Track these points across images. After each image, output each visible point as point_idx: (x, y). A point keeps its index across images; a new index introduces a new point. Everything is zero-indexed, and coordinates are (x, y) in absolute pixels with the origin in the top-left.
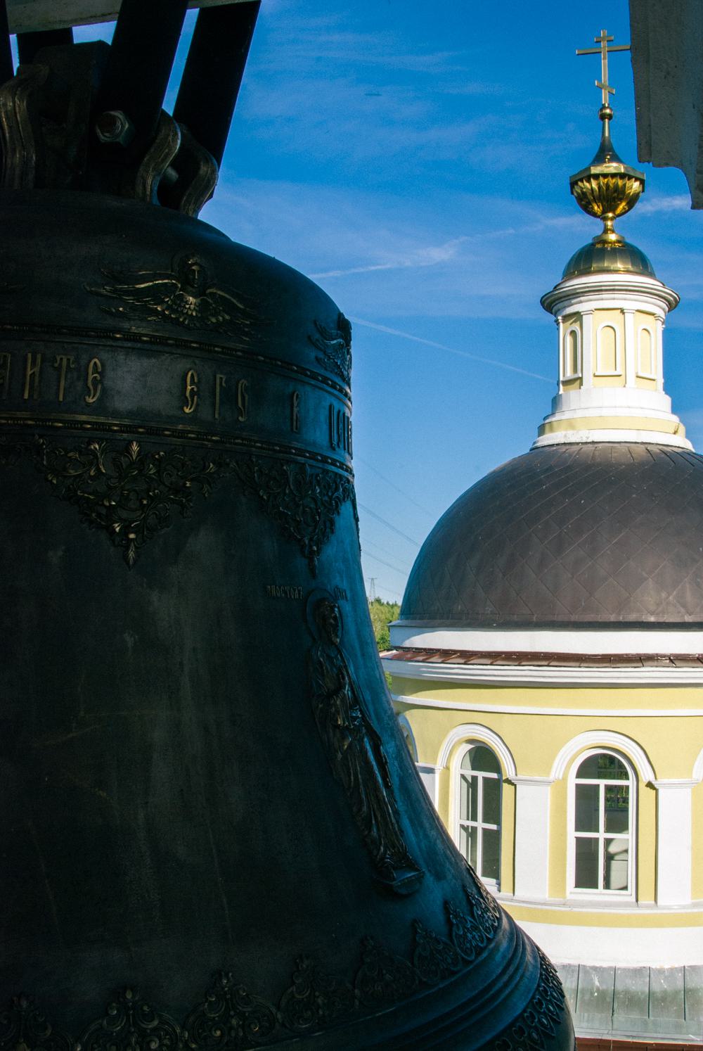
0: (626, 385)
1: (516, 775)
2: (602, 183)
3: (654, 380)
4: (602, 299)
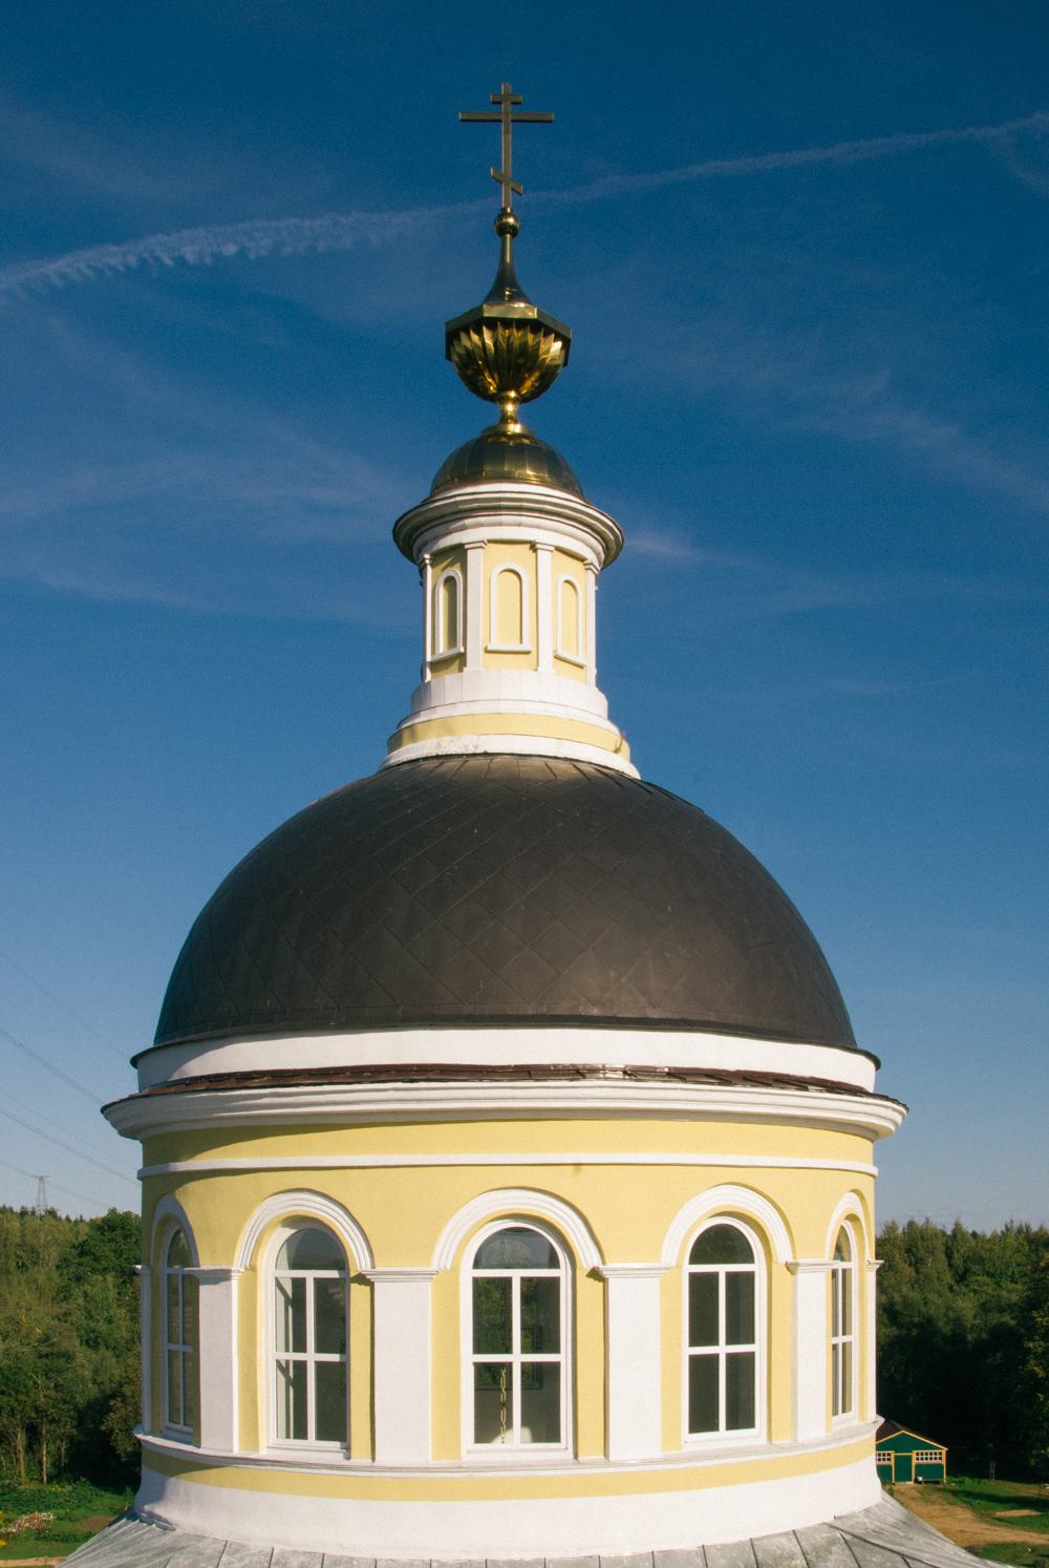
0: (539, 668)
1: (373, 1267)
2: (500, 338)
3: (582, 667)
4: (500, 524)
